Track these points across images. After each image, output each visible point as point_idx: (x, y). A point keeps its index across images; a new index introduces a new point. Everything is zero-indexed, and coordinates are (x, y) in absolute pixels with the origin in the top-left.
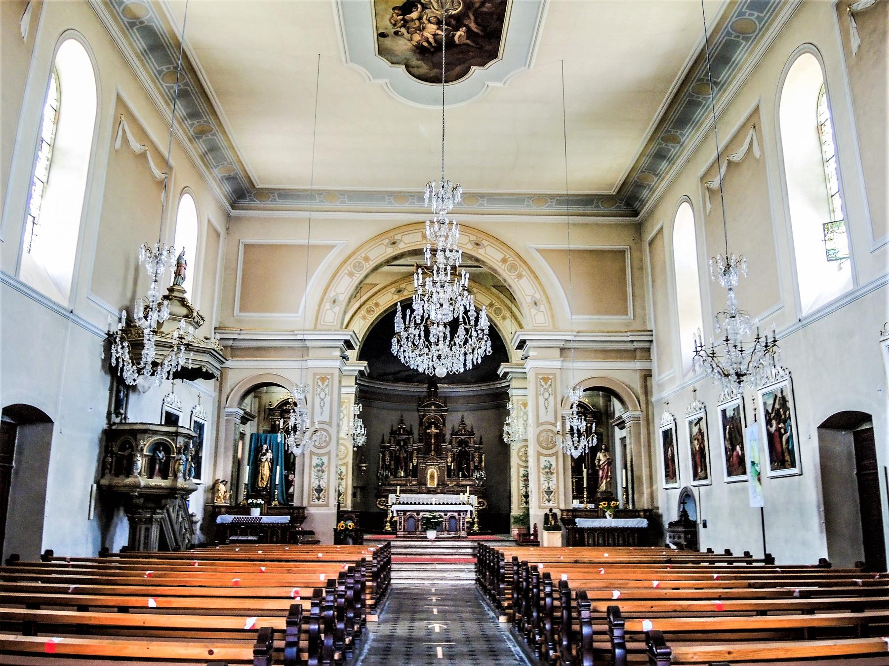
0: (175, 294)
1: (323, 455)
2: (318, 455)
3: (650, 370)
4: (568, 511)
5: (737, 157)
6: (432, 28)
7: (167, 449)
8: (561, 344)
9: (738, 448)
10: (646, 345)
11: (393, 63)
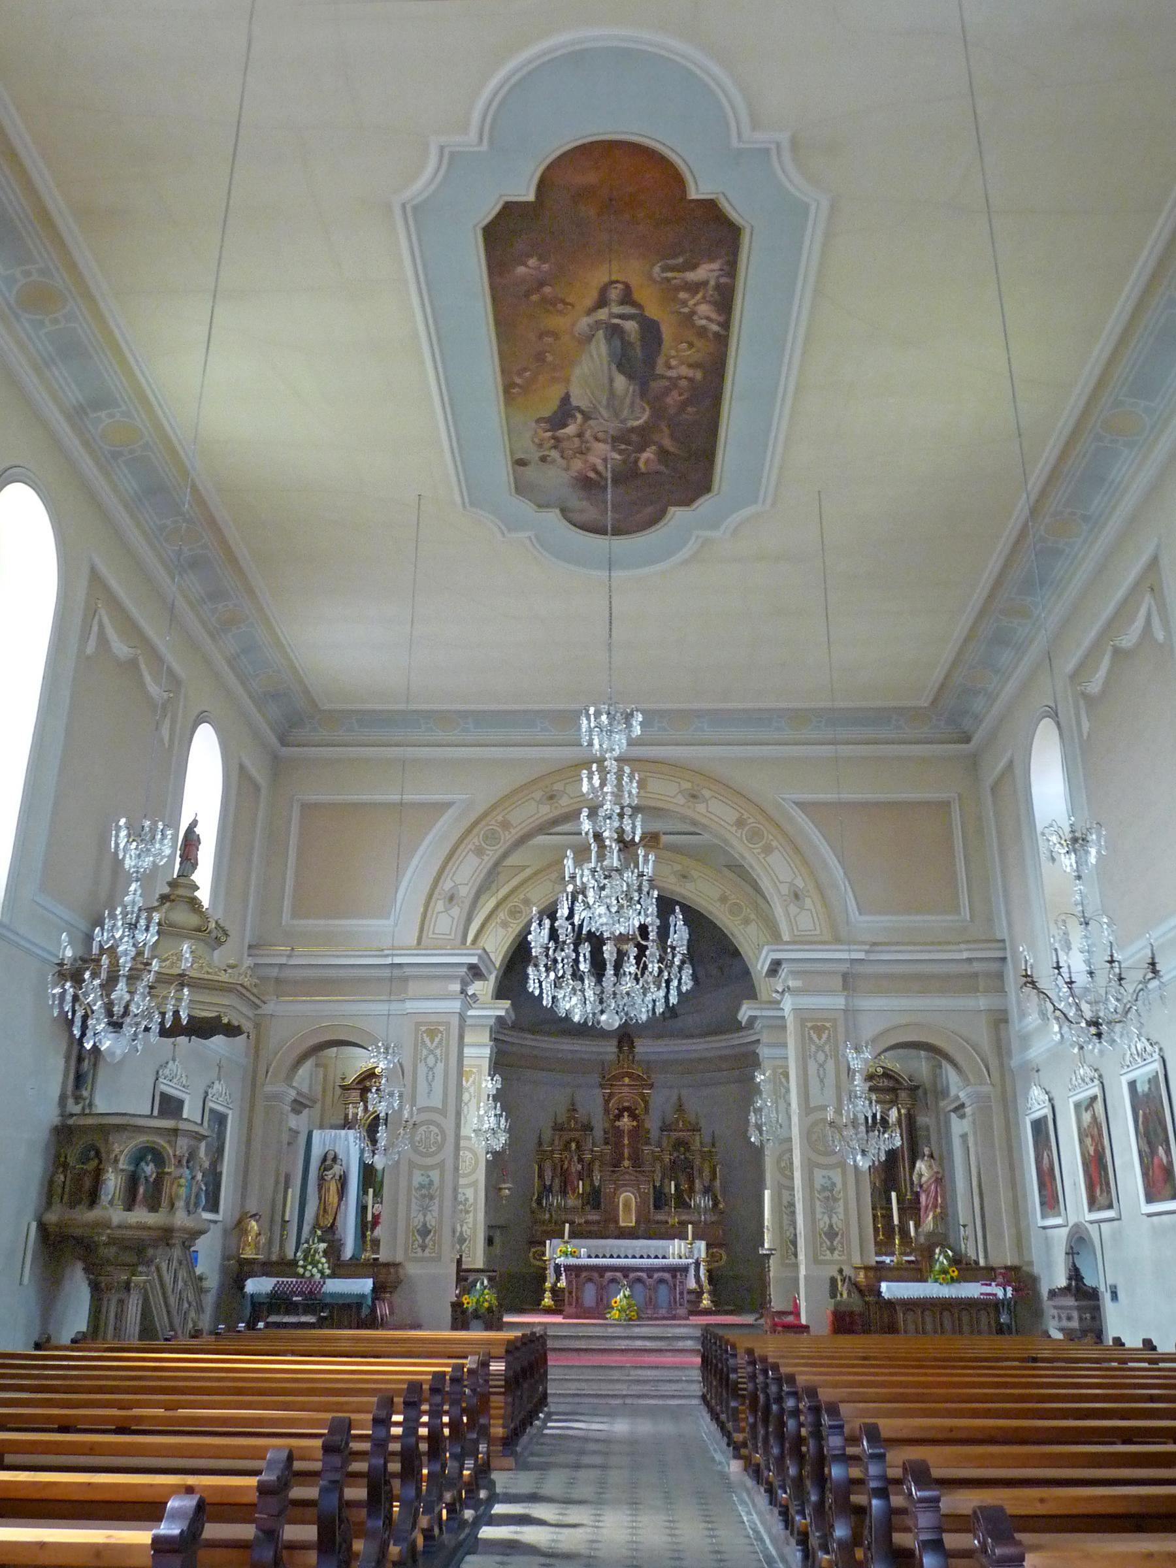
0: (181, 891)
1: (431, 1167)
2: (421, 1167)
3: (1005, 1011)
4: (867, 1268)
5: (1128, 640)
6: (602, 448)
7: (159, 1158)
8: (844, 967)
9: (1161, 1151)
10: (994, 967)
11: (539, 506)
